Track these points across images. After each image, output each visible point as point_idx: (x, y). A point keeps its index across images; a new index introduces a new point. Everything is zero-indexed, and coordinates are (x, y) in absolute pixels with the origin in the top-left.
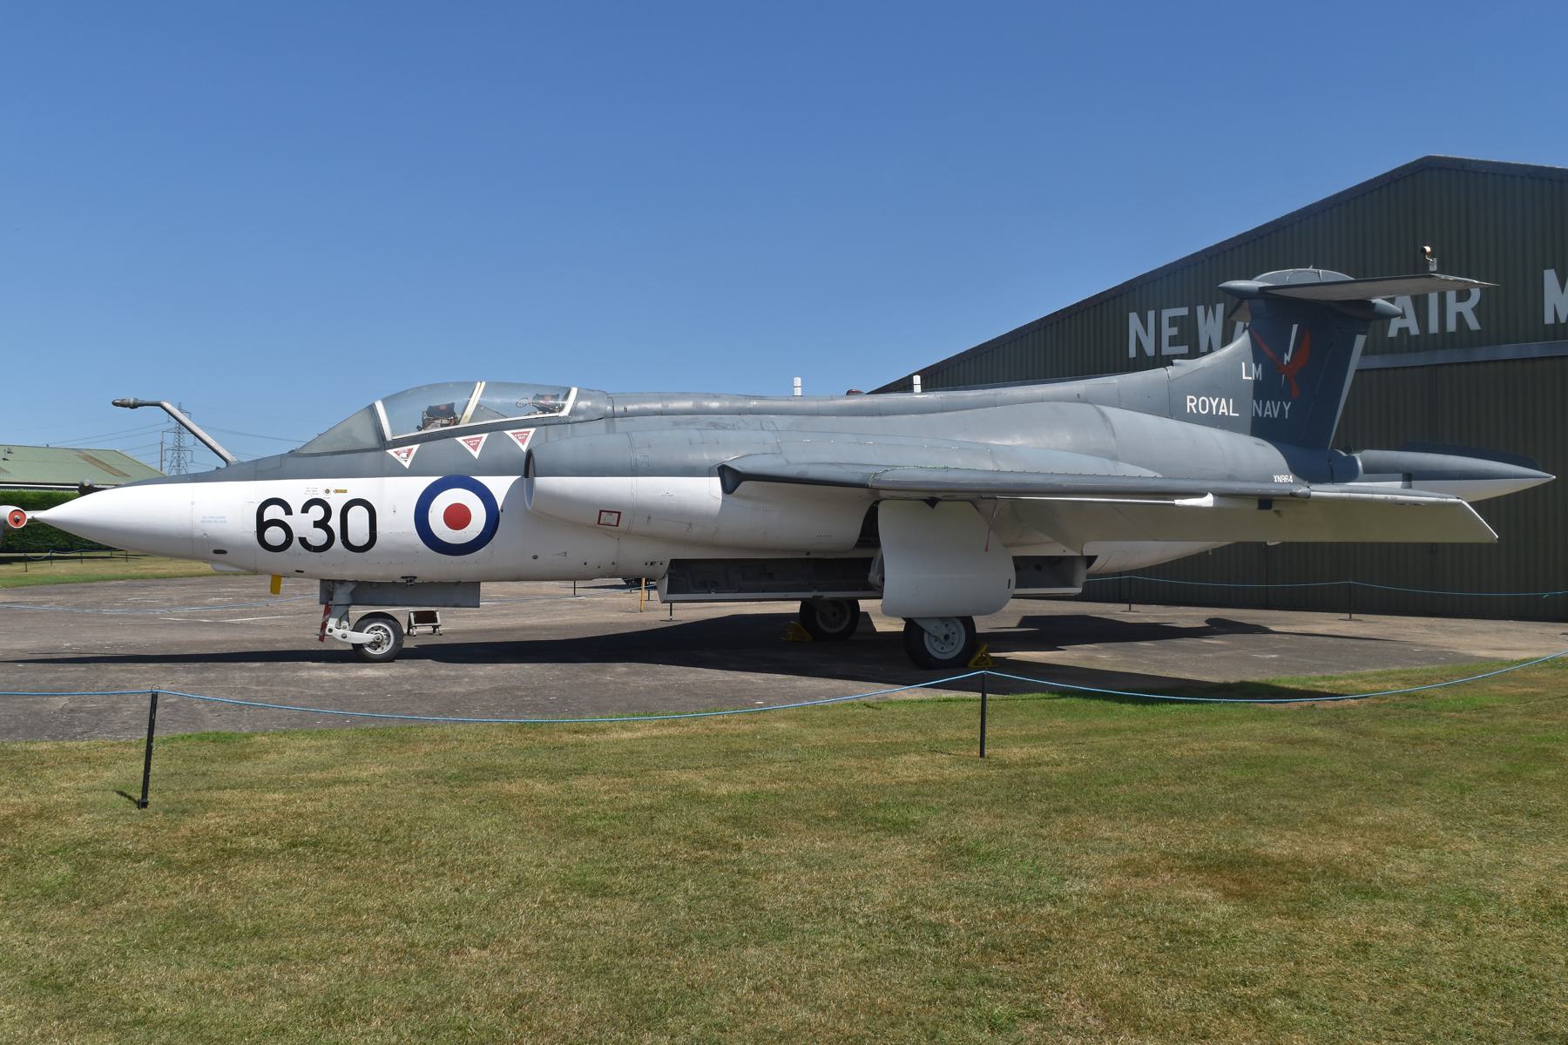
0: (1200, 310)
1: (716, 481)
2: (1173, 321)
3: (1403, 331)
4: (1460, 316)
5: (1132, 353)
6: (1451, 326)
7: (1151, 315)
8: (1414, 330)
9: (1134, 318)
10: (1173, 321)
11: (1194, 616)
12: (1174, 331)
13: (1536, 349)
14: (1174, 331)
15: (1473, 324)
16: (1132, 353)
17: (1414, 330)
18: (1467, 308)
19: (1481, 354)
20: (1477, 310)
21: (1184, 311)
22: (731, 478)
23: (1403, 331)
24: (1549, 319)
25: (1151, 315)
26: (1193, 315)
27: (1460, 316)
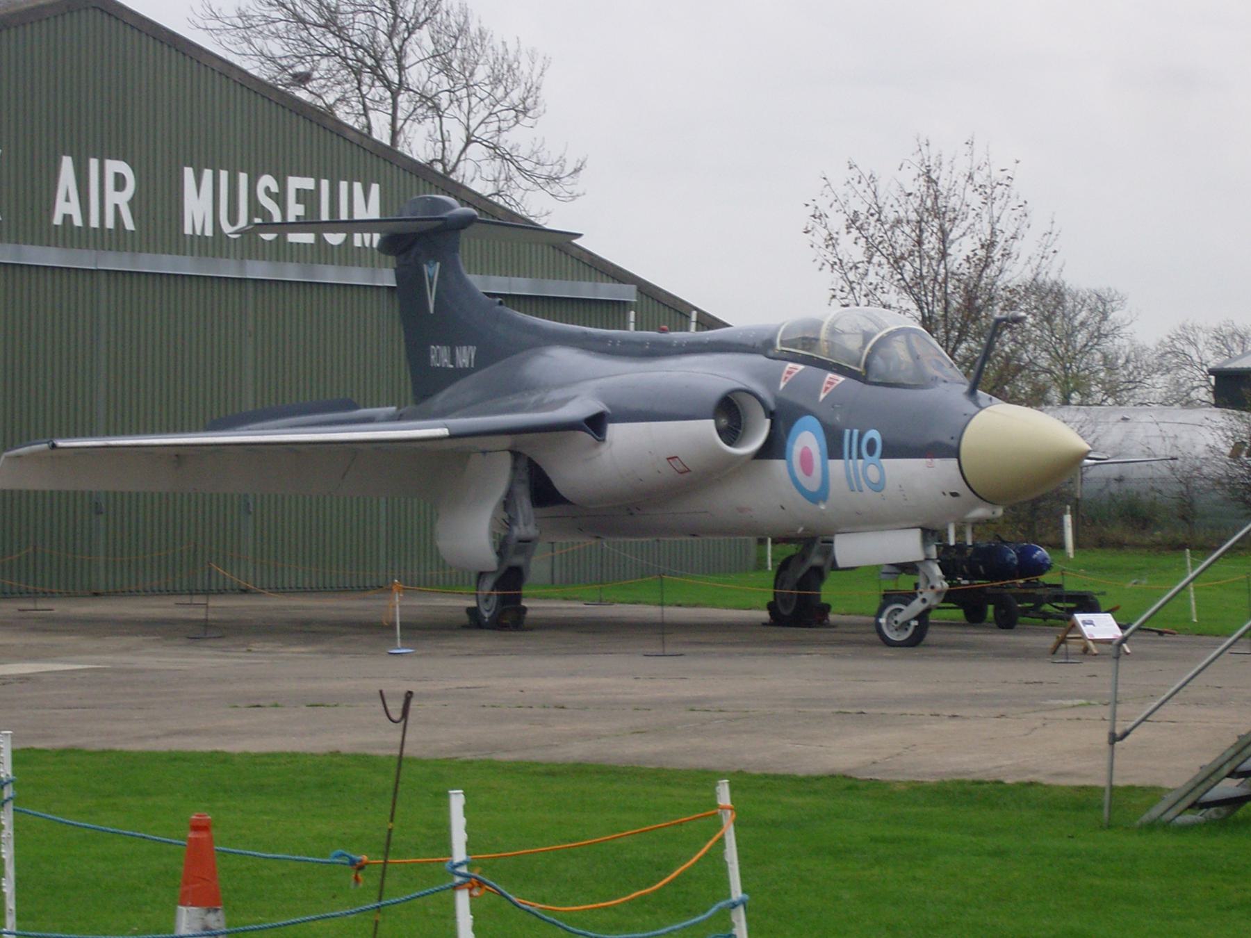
3: (67, 218)
4: (117, 206)
8: (78, 222)
9: (189, 173)
15: (129, 225)
18: (122, 199)
20: (131, 203)
23: (67, 218)
24: (188, 230)
27: (117, 206)
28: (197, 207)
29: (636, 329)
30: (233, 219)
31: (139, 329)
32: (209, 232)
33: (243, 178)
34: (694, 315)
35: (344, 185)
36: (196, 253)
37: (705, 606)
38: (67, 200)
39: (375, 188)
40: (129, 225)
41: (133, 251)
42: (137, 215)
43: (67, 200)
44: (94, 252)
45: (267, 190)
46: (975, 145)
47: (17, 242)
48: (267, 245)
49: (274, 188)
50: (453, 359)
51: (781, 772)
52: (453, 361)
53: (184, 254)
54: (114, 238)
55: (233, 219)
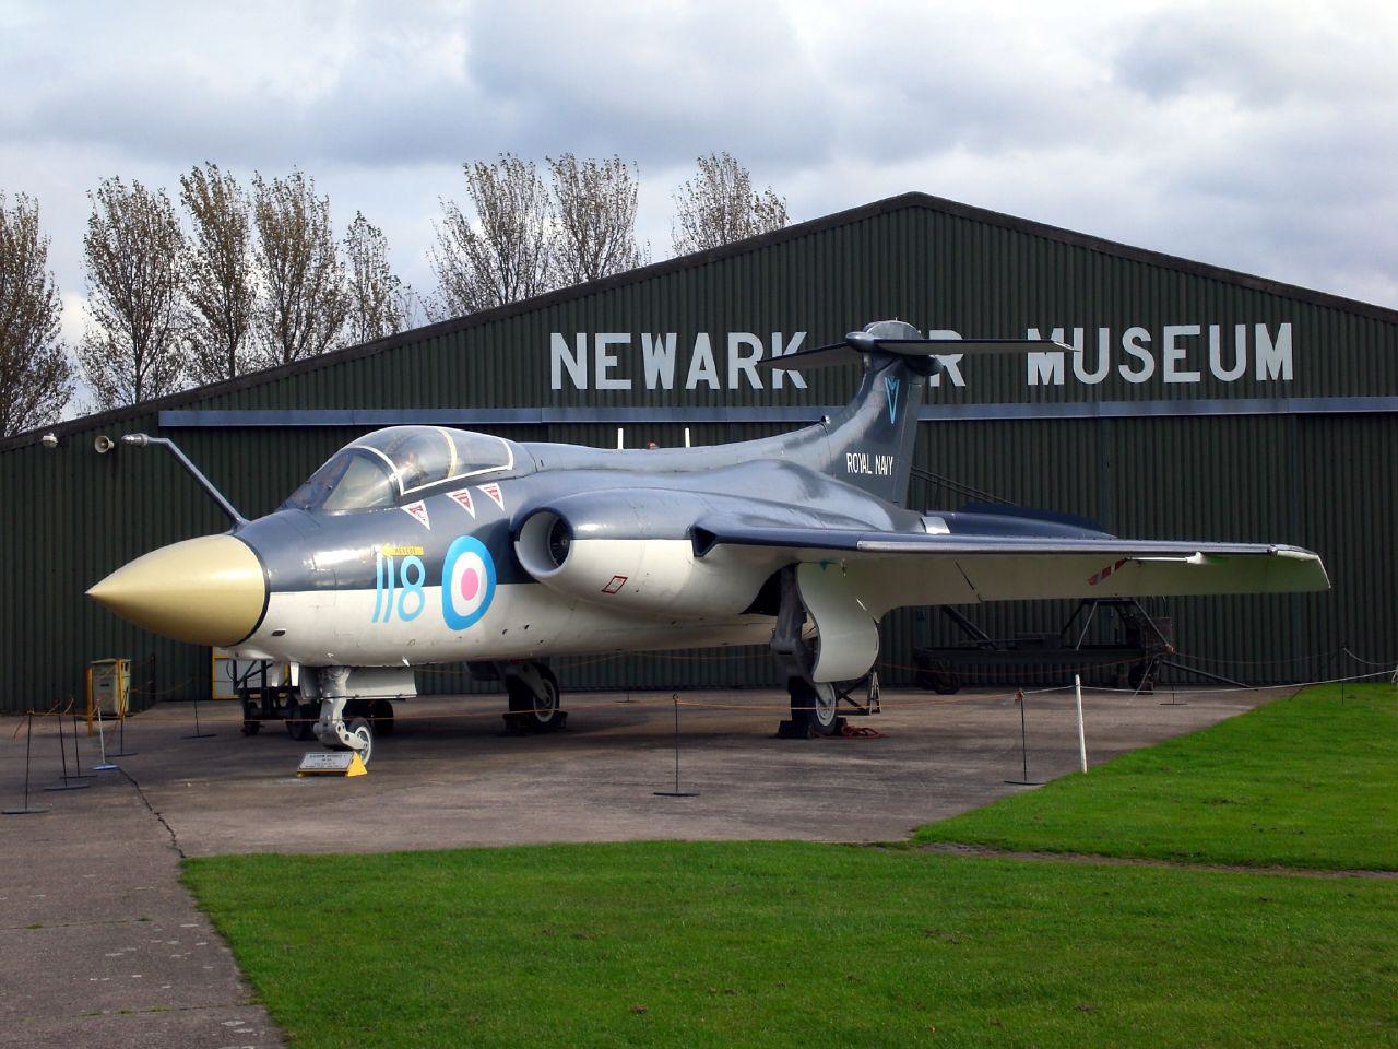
0: (646, 338)
1: (688, 544)
2: (611, 349)
3: (703, 384)
4: (742, 372)
5: (556, 384)
6: (734, 383)
7: (581, 338)
8: (714, 384)
10: (611, 349)
11: (931, 734)
12: (1182, 354)
13: (1023, 411)
14: (1182, 354)
15: (958, 380)
16: (556, 384)
17: (714, 384)
19: (971, 412)
21: (625, 338)
22: (702, 539)
23: (703, 384)
24: (1032, 380)
25: (581, 338)
26: (637, 341)
27: (742, 372)
28: (1043, 366)
29: (624, 448)
30: (1091, 365)
31: (939, 448)
32: (1059, 380)
33: (1104, 334)
35: (1241, 330)
36: (1090, 399)
38: (703, 368)
39: (1286, 330)
41: (560, 405)
42: (969, 371)
43: (703, 368)
44: (815, 407)
45: (1137, 341)
46: (711, 525)
47: (817, 404)
48: (1091, 389)
49: (1145, 336)
50: (872, 466)
52: (872, 466)
53: (643, 405)
54: (1275, 388)
55: (1091, 365)
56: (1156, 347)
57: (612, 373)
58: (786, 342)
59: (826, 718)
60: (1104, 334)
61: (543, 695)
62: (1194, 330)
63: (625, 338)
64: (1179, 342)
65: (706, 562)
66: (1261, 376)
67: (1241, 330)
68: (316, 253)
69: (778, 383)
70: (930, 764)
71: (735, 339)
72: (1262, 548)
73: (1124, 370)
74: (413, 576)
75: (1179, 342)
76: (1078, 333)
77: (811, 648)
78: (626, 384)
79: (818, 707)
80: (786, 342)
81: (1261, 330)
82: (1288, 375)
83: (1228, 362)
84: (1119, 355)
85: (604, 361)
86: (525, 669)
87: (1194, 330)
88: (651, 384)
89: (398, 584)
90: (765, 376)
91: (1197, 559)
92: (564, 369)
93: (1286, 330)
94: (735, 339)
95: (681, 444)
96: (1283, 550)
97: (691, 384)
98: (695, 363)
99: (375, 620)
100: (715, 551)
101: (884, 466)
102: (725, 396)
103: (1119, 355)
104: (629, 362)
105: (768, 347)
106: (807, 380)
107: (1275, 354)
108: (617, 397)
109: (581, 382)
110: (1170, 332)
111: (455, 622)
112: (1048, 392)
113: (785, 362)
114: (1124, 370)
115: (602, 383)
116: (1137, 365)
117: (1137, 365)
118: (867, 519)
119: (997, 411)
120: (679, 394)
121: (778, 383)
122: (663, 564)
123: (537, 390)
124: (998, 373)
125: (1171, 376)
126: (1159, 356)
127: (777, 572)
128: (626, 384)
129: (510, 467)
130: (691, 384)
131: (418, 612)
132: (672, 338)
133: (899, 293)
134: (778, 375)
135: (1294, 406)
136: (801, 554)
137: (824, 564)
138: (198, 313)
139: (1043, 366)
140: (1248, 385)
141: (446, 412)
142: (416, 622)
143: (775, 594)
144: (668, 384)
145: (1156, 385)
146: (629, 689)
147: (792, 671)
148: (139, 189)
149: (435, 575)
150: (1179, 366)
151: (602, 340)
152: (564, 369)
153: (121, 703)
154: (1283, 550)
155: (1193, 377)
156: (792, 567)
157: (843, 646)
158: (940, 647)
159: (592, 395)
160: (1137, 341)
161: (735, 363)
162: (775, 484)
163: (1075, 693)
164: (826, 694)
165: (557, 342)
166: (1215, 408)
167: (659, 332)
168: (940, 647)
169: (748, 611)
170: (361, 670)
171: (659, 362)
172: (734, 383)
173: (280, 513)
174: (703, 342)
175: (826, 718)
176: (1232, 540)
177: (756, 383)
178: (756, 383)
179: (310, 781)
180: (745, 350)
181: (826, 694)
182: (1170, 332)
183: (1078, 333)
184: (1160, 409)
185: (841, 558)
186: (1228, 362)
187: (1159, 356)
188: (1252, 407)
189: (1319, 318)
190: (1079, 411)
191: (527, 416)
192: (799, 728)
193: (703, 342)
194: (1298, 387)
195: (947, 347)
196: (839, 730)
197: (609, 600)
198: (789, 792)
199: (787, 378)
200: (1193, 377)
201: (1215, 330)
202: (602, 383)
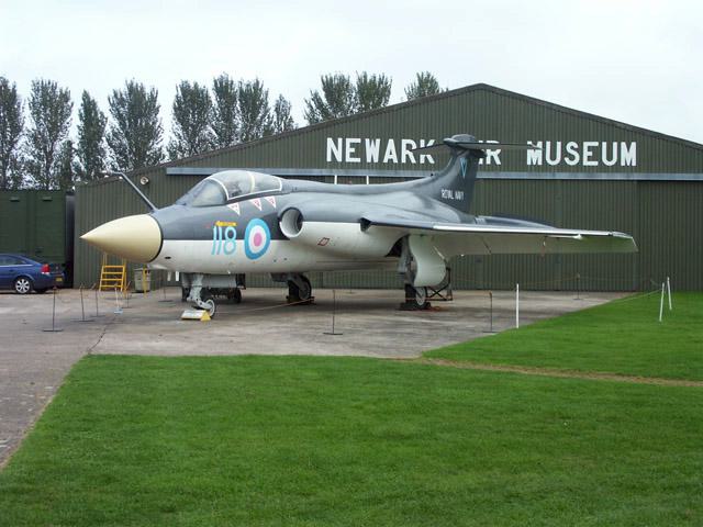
0: (367, 141)
4: (492, 157)
5: (329, 159)
6: (404, 161)
7: (340, 140)
8: (396, 161)
10: (352, 145)
12: (591, 154)
13: (525, 176)
15: (498, 162)
16: (329, 159)
17: (396, 161)
19: (503, 175)
21: (359, 141)
22: (365, 224)
24: (529, 163)
25: (340, 140)
26: (363, 141)
27: (492, 157)
28: (534, 156)
30: (553, 157)
32: (540, 163)
33: (559, 144)
34: (105, 255)
35: (615, 144)
37: (390, 288)
39: (634, 145)
40: (498, 162)
45: (572, 148)
46: (369, 217)
49: (576, 146)
50: (454, 196)
51: (114, 353)
52: (454, 196)
54: (628, 169)
55: (553, 157)
56: (580, 150)
57: (352, 155)
58: (427, 142)
59: (421, 302)
60: (559, 144)
61: (304, 289)
62: (596, 144)
63: (359, 141)
64: (589, 149)
65: (368, 233)
66: (623, 164)
67: (615, 144)
68: (262, 111)
69: (422, 161)
70: (456, 323)
71: (405, 142)
72: (607, 233)
73: (567, 159)
74: (231, 235)
75: (589, 149)
76: (548, 144)
77: (413, 275)
78: (358, 160)
79: (418, 298)
80: (427, 142)
81: (623, 144)
82: (634, 164)
83: (610, 158)
84: (565, 153)
85: (349, 150)
86: (295, 278)
87: (596, 144)
88: (369, 160)
89: (224, 238)
90: (417, 158)
91: (579, 237)
92: (333, 153)
93: (634, 145)
94: (405, 142)
95: (365, 183)
96: (615, 234)
97: (386, 161)
98: (387, 152)
99: (213, 253)
100: (371, 228)
101: (459, 195)
102: (400, 166)
103: (565, 153)
104: (360, 151)
105: (418, 144)
106: (434, 159)
107: (629, 155)
108: (355, 165)
109: (339, 159)
110: (586, 144)
111: (251, 256)
112: (535, 168)
113: (426, 150)
114: (567, 159)
115: (348, 159)
116: (572, 158)
117: (572, 158)
118: (448, 221)
119: (514, 175)
120: (380, 165)
121: (422, 161)
122: (350, 234)
123: (322, 163)
124: (515, 159)
125: (586, 163)
126: (581, 154)
127: (400, 241)
128: (358, 160)
129: (280, 189)
130: (386, 161)
131: (233, 251)
132: (378, 141)
133: (470, 128)
134: (422, 157)
135: (636, 177)
136: (411, 231)
137: (422, 235)
138: (214, 133)
139: (534, 156)
140: (617, 167)
141: (272, 170)
142: (233, 255)
143: (398, 249)
144: (376, 160)
145: (579, 167)
146: (351, 288)
147: (406, 282)
148: (196, 85)
149: (241, 236)
150: (589, 159)
151: (349, 141)
152: (333, 153)
153: (146, 287)
154: (615, 234)
155: (595, 163)
156: (407, 236)
157: (427, 271)
158: (475, 268)
159: (344, 164)
160: (572, 148)
161: (405, 152)
162: (399, 205)
163: (515, 298)
164: (421, 292)
165: (330, 141)
166: (604, 176)
167: (373, 138)
168: (475, 268)
169: (389, 255)
170: (207, 276)
171: (372, 151)
172: (404, 161)
173: (174, 206)
174: (391, 142)
175: (421, 302)
176: (593, 230)
177: (413, 161)
178: (413, 161)
179: (183, 322)
180: (409, 147)
181: (421, 292)
182: (586, 144)
183: (548, 144)
184: (581, 176)
185: (426, 234)
186: (610, 158)
187: (581, 154)
188: (619, 176)
189: (654, 145)
190: (548, 176)
191: (316, 172)
192: (409, 305)
193: (391, 142)
194: (637, 169)
195: (493, 148)
196: (427, 307)
197: (321, 247)
198: (383, 334)
199: (426, 158)
200: (595, 163)
201: (604, 144)
202: (348, 159)
